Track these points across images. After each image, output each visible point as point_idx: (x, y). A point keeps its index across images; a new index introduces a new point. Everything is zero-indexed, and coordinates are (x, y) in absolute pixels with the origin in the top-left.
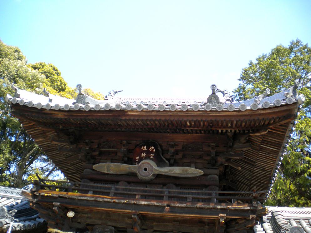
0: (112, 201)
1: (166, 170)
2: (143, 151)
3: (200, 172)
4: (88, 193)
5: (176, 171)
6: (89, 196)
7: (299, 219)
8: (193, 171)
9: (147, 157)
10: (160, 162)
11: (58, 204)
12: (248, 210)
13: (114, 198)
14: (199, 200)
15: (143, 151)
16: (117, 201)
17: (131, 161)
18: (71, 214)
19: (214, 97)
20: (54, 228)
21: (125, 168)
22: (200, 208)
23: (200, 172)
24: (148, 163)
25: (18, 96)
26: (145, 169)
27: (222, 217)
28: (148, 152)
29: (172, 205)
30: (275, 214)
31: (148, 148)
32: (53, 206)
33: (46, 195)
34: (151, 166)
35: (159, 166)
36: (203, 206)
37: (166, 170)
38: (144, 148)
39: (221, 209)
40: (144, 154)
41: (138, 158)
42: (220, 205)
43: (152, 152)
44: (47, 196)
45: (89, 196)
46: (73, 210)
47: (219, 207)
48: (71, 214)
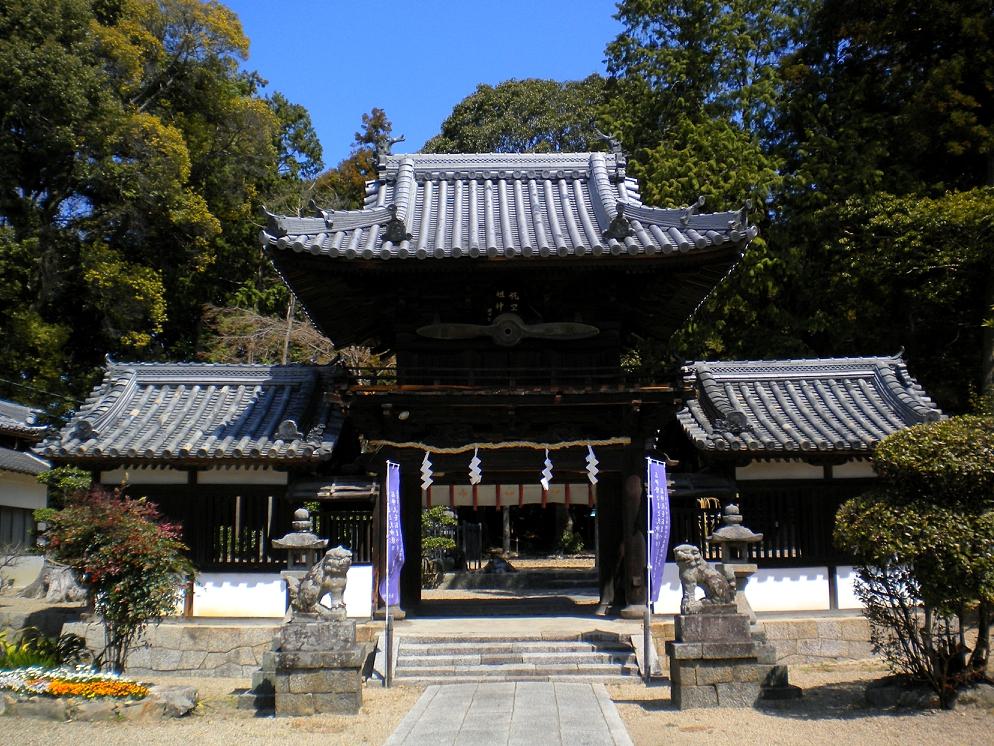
0: (476, 393)
1: (538, 330)
2: (500, 300)
3: (594, 330)
4: (432, 384)
5: (557, 329)
6: (436, 390)
7: (739, 382)
8: (583, 329)
9: (507, 309)
10: (529, 318)
11: (389, 405)
12: (671, 392)
13: (477, 387)
14: (602, 382)
15: (500, 300)
16: (483, 393)
17: (480, 318)
18: (404, 415)
19: (621, 223)
20: (379, 439)
21: (474, 329)
22: (605, 394)
23: (594, 330)
24: (514, 323)
25: (284, 233)
26: (508, 331)
27: (636, 404)
28: (507, 301)
29: (566, 392)
30: (702, 377)
31: (507, 294)
32: (383, 409)
33: (366, 393)
34: (517, 326)
35: (527, 321)
36: (610, 391)
37: (538, 330)
38: (501, 294)
39: (634, 393)
40: (501, 305)
41: (490, 310)
42: (633, 387)
43: (515, 301)
44: (369, 395)
45: (436, 390)
46: (404, 409)
47: (632, 391)
48: (404, 415)
